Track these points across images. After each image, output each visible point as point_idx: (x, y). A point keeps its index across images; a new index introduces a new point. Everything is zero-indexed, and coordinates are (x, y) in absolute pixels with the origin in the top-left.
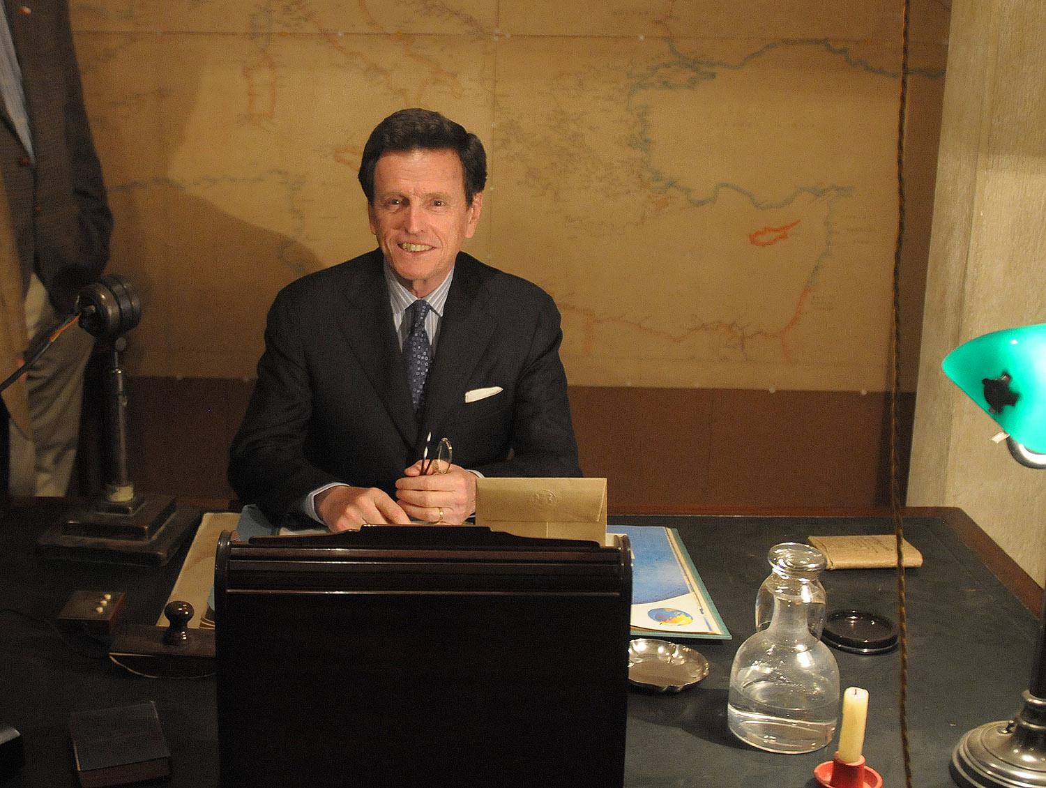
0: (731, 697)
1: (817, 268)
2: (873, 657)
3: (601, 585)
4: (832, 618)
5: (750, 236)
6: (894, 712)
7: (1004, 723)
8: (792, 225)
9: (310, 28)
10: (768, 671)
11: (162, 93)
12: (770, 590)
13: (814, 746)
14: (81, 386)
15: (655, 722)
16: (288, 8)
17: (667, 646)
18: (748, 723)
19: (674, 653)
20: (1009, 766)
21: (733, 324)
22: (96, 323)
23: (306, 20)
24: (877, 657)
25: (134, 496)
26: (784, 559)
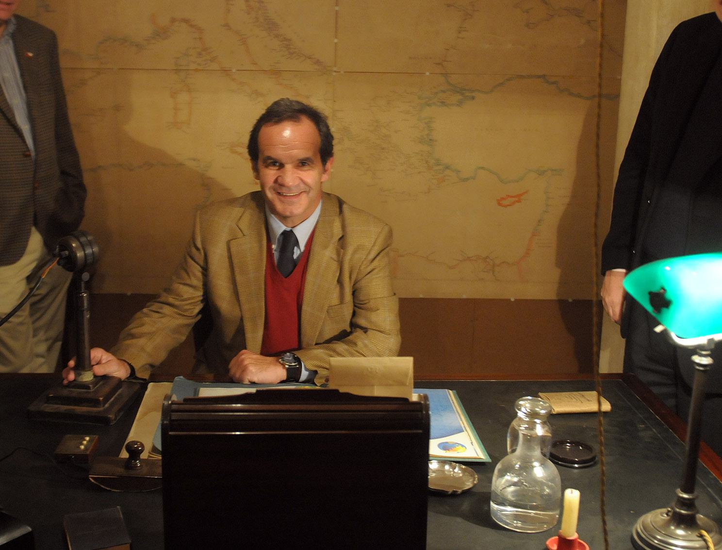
0: (492, 498)
1: (539, 221)
3: (410, 428)
4: (554, 445)
5: (498, 200)
6: (596, 505)
7: (664, 510)
8: (523, 194)
9: (214, 66)
10: (516, 479)
11: (117, 108)
12: (517, 428)
14: (65, 299)
15: (445, 514)
16: (200, 54)
17: (450, 465)
18: (503, 512)
19: (455, 469)
20: (667, 537)
21: (487, 257)
22: (69, 263)
24: (586, 469)
26: (525, 407)
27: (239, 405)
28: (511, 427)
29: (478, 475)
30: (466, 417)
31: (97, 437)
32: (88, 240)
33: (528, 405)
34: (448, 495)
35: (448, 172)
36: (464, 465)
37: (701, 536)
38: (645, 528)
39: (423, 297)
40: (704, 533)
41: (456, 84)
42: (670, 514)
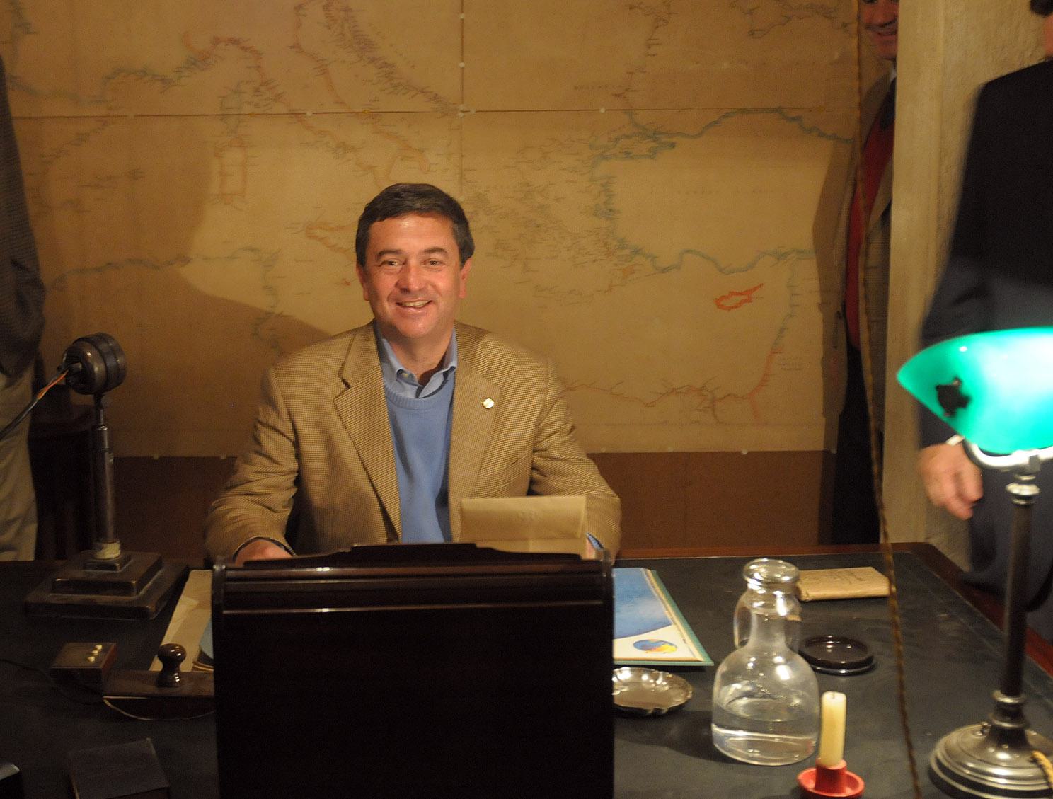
0: (715, 718)
1: (782, 330)
2: (849, 678)
3: (574, 605)
7: (978, 727)
8: (756, 289)
9: (279, 108)
10: (749, 688)
11: (134, 175)
13: (796, 758)
16: (257, 90)
18: (733, 739)
20: (981, 763)
21: (704, 387)
23: (275, 100)
25: (121, 553)
26: (760, 573)
27: (327, 569)
28: (738, 606)
30: (672, 606)
31: (113, 645)
33: (763, 570)
34: (647, 717)
37: (1035, 761)
38: (949, 752)
40: (1039, 755)
42: (986, 731)
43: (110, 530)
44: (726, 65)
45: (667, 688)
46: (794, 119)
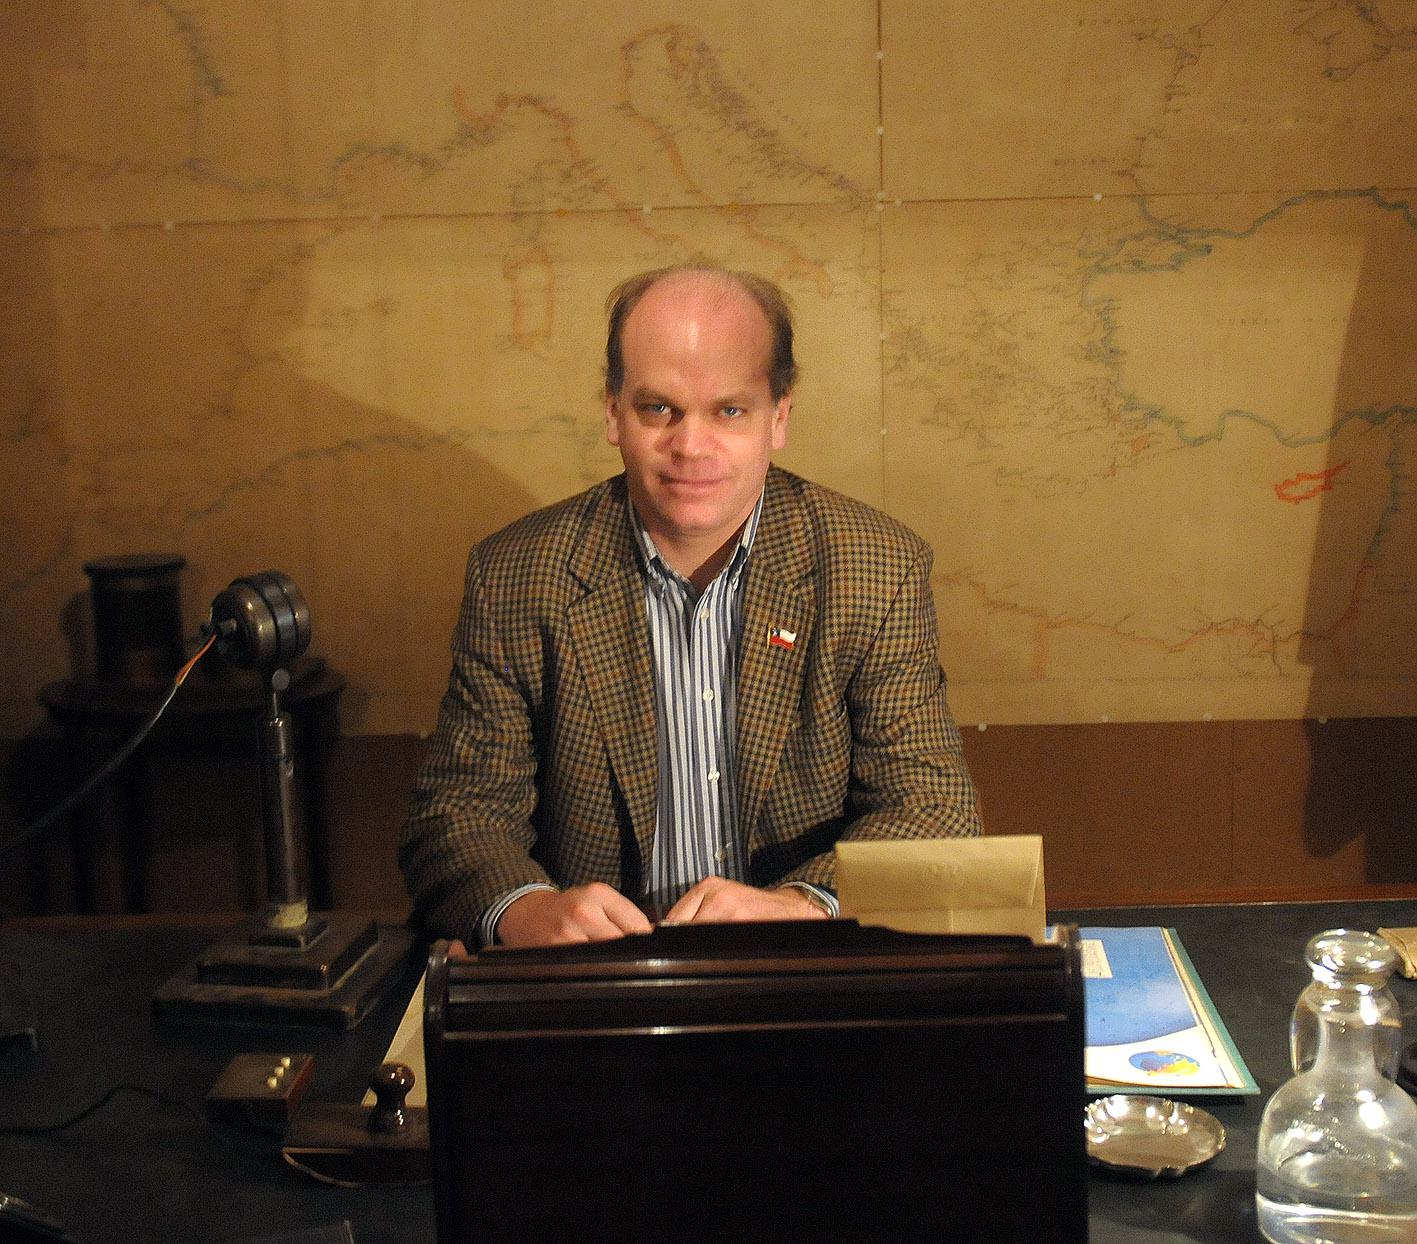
0: (1261, 1181)
1: (1379, 533)
3: (1027, 1014)
9: (601, 201)
10: (1316, 1136)
11: (383, 307)
12: (1312, 1007)
17: (1159, 1106)
23: (595, 190)
29: (1225, 1128)
32: (285, 596)
35: (1156, 425)
36: (1191, 1104)
39: (1112, 720)
41: (1171, 228)
43: (291, 883)
44: (1288, 124)
45: (1185, 1130)
46: (1396, 206)
